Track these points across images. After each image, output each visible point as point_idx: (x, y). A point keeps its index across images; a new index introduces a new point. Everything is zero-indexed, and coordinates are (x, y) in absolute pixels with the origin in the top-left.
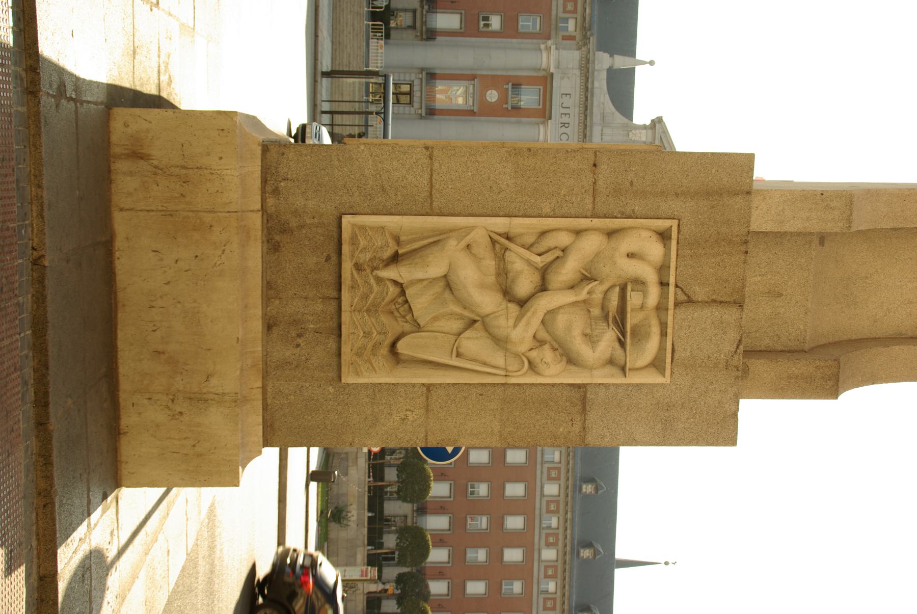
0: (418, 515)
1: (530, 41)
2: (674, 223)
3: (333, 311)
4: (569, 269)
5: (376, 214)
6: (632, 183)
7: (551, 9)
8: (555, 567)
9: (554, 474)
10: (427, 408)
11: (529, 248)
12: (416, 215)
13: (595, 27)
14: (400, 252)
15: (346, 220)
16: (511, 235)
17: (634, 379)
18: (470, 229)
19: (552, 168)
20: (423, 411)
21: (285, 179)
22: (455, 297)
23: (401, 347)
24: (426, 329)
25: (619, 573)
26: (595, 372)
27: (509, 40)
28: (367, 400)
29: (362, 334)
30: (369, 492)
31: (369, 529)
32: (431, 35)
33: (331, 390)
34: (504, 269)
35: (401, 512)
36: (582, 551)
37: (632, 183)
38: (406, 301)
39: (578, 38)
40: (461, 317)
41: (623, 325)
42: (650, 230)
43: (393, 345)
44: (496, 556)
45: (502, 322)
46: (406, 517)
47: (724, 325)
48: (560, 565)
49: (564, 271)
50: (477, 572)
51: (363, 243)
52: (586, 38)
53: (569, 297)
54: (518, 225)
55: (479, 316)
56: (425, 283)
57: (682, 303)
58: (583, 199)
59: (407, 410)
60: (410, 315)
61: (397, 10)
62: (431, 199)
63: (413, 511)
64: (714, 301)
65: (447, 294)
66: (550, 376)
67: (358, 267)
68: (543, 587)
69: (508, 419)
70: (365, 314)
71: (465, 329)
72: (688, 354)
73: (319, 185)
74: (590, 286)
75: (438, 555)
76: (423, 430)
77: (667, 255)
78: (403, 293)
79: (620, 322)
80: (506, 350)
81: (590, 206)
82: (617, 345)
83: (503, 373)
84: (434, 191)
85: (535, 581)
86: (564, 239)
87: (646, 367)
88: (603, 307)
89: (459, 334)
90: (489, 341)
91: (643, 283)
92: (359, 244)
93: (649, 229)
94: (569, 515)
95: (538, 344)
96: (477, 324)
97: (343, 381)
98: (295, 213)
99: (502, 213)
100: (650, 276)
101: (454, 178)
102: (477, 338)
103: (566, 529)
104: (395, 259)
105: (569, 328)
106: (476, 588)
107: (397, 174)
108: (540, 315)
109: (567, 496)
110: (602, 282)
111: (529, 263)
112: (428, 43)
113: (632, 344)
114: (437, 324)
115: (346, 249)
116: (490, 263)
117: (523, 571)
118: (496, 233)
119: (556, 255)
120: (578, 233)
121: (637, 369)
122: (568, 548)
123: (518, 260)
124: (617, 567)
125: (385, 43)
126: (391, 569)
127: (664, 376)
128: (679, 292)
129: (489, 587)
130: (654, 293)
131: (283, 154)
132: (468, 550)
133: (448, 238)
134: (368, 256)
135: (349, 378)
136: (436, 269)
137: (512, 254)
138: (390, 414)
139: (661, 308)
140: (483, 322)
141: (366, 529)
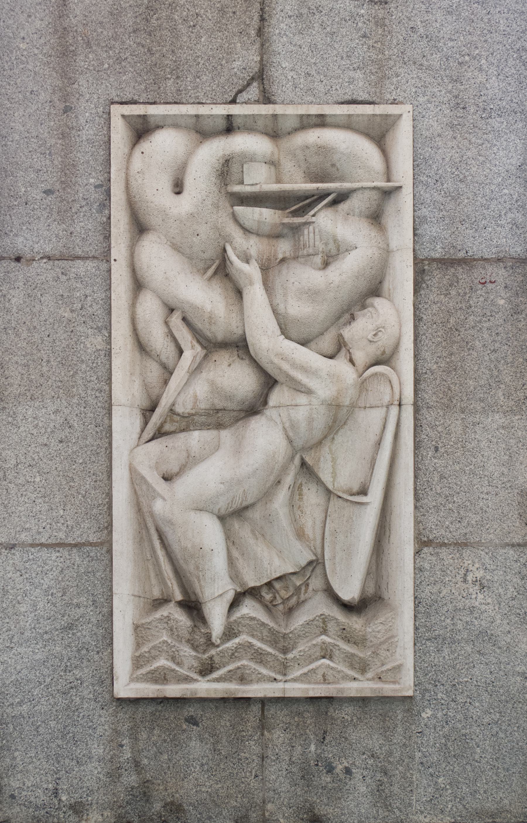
3: (285, 712)
4: (202, 296)
11: (168, 372)
14: (179, 597)
15: (125, 687)
16: (146, 404)
18: (136, 479)
19: (25, 335)
20: (466, 553)
21: (56, 793)
23: (350, 592)
24: (319, 551)
28: (446, 651)
33: (427, 713)
34: (208, 415)
38: (269, 584)
40: (297, 490)
41: (307, 198)
42: (130, 155)
43: (347, 607)
45: (300, 415)
47: (305, 11)
49: (208, 307)
51: (163, 662)
53: (256, 295)
54: (126, 389)
55: (292, 458)
56: (235, 554)
58: (78, 277)
59: (465, 581)
60: (294, 578)
62: (84, 544)
64: (260, 32)
65: (255, 514)
67: (206, 669)
69: (482, 400)
70: (290, 656)
71: (319, 482)
72: (359, 74)
73: (63, 737)
77: (175, 123)
78: (253, 593)
79: (298, 204)
80: (353, 406)
81: (90, 265)
82: (343, 207)
83: (394, 410)
84: (70, 540)
86: (149, 308)
89: (329, 492)
90: (339, 439)
92: (164, 668)
95: (343, 351)
96: (307, 459)
97: (410, 693)
98: (114, 775)
99: (106, 421)
101: (46, 507)
102: (334, 460)
104: (193, 607)
105: (313, 294)
107: (41, 605)
108: (290, 347)
111: (196, 370)
113: (342, 179)
114: (309, 531)
115: (173, 690)
116: (196, 438)
118: (142, 431)
123: (191, 391)
127: (401, 115)
131: (13, 797)
133: (152, 515)
134: (187, 651)
135: (406, 685)
136: (210, 534)
137: (180, 400)
138: (472, 610)
139: (274, 132)
140: (304, 449)
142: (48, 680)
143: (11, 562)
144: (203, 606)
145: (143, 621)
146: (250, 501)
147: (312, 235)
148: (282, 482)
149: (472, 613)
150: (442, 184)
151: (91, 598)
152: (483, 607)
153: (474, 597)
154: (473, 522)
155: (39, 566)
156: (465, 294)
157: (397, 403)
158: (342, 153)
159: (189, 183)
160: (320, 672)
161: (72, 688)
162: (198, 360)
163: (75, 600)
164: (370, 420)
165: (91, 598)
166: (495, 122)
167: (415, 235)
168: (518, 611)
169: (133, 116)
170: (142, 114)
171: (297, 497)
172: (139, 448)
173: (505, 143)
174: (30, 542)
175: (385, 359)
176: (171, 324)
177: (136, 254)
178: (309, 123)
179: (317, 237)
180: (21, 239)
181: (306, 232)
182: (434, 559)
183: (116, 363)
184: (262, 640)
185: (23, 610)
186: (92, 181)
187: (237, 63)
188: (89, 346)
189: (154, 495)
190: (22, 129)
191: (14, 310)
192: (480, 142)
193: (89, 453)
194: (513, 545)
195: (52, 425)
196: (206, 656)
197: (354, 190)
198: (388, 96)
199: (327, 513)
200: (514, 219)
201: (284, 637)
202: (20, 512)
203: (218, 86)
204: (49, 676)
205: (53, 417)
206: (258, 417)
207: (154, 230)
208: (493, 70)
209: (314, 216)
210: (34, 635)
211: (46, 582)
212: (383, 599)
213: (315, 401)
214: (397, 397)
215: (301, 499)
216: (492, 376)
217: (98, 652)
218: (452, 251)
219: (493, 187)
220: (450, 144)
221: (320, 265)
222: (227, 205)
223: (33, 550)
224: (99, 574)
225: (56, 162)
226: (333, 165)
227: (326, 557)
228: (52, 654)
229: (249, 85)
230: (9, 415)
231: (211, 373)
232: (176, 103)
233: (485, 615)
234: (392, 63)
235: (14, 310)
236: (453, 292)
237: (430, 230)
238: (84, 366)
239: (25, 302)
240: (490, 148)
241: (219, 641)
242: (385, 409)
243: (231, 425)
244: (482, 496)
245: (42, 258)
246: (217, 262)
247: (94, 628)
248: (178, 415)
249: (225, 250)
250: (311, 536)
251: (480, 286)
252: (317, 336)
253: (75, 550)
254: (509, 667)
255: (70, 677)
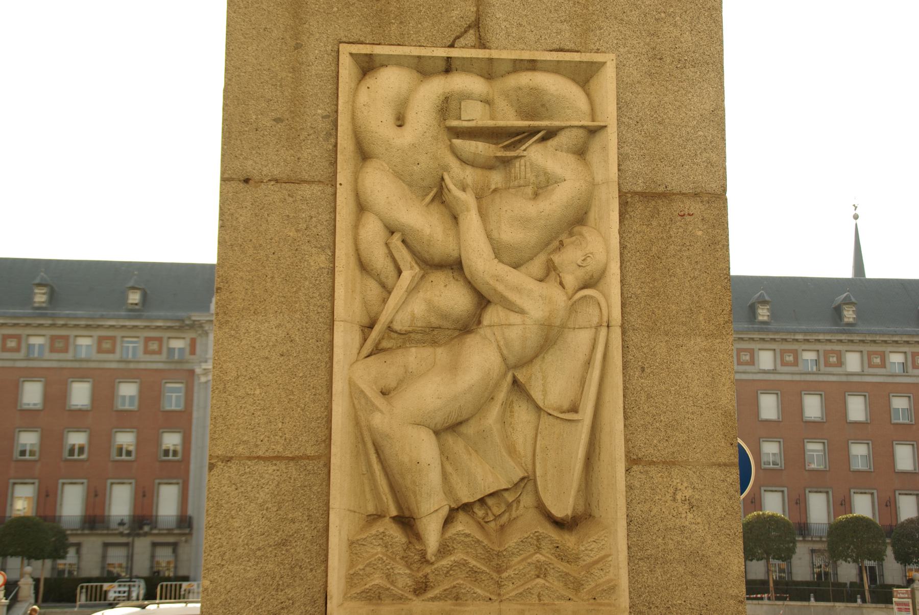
0: (809, 534)
1: (195, 395)
2: (345, 49)
5: (327, 556)
6: (278, 120)
7: (156, 370)
8: (870, 354)
9: (746, 357)
10: (669, 464)
11: (387, 290)
12: (328, 485)
13: (182, 314)
14: (394, 512)
16: (366, 321)
17: (609, 112)
20: (675, 471)
22: (473, 416)
23: (561, 510)
24: (530, 467)
25: (871, 273)
26: (599, 178)
27: (194, 421)
28: (659, 571)
29: (540, 581)
30: (785, 599)
31: (835, 600)
32: (185, 522)
34: (424, 332)
35: (807, 558)
36: (846, 320)
37: (278, 120)
38: (482, 501)
39: (193, 335)
40: (508, 406)
43: (559, 524)
44: (859, 431)
45: (514, 334)
46: (813, 551)
48: (866, 348)
49: (427, 231)
50: (883, 456)
51: (377, 580)
52: (194, 326)
53: (472, 221)
54: (348, 304)
55: (505, 375)
56: (449, 469)
57: (480, 38)
58: (303, 199)
59: (674, 500)
60: (506, 494)
61: (152, 567)
62: (301, 458)
63: (804, 541)
65: (469, 430)
66: (608, 252)
68: (898, 370)
70: (505, 575)
71: (530, 398)
72: (565, 26)
74: (451, 187)
75: (863, 506)
76: (709, 471)
78: (466, 507)
79: (512, 138)
80: (563, 327)
81: (316, 188)
83: (603, 332)
84: (288, 454)
85: (890, 380)
86: (372, 230)
87: (588, 95)
88: (488, 166)
89: (538, 409)
90: (549, 357)
91: (447, 99)
92: (380, 587)
93: (355, 92)
94: (799, 337)
95: (553, 274)
96: (521, 378)
99: (327, 336)
100: (436, 87)
102: (544, 378)
103: (819, 341)
104: (407, 522)
105: (524, 222)
106: (904, 458)
107: (255, 520)
108: (503, 270)
109: (774, 340)
110: (446, 168)
111: (413, 290)
112: (195, 526)
113: (550, 118)
114: (520, 448)
116: (414, 356)
117: (878, 396)
118: (362, 346)
119: (399, 244)
120: (361, 207)
121: (593, 109)
122: (843, 337)
123: (409, 309)
124: (864, 275)
125: (195, 580)
126: (887, 573)
127: (605, 63)
128: (462, 41)
129: (903, 441)
130: (461, 82)
132: (853, 468)
133: (370, 429)
134: (401, 569)
136: (424, 449)
137: (399, 318)
138: (682, 529)
139: (489, 71)
140: (516, 367)
141: (837, 604)
142: (259, 600)
143: (227, 475)
144: (418, 522)
145: (358, 538)
146: (465, 416)
147: (523, 168)
148: (496, 398)
149: (682, 532)
150: (643, 126)
151: (306, 513)
152: (693, 527)
153: (683, 516)
154: (680, 441)
155: (255, 480)
156: (666, 225)
157: (605, 324)
158: (552, 95)
159: (411, 116)
160: (535, 591)
161: (283, 608)
162: (416, 279)
163: (291, 515)
164: (580, 340)
165: (306, 513)
166: (689, 72)
167: (619, 170)
168: (728, 532)
169: (360, 54)
170: (368, 52)
171: (509, 414)
172: (359, 363)
173: (699, 91)
174: (247, 454)
175: (592, 282)
176: (392, 246)
177: (360, 180)
178: (519, 66)
179: (528, 170)
180: (250, 162)
181: (517, 165)
182: (643, 477)
183: (340, 280)
184: (476, 557)
185: (236, 525)
186: (319, 111)
188: (312, 264)
189: (375, 408)
190: (255, 62)
191: (241, 228)
192: (676, 89)
193: (309, 367)
194: (719, 465)
195: (273, 339)
196: (420, 574)
197: (561, 129)
198: (592, 46)
199: (537, 430)
200: (708, 158)
201: (498, 555)
202: (239, 424)
203: (438, 31)
204: (260, 595)
205: (275, 331)
206: (472, 335)
207: (377, 158)
208: (686, 26)
209: (525, 150)
210: (246, 551)
211: (262, 496)
212: (594, 517)
213: (528, 321)
214: (605, 319)
215: (512, 416)
216: (693, 301)
217: (311, 570)
218: (653, 186)
219: (689, 129)
220: (648, 90)
221: (531, 196)
222: (446, 138)
223: (249, 463)
224: (315, 488)
225: (286, 94)
226: (543, 105)
227: (538, 474)
228: (265, 572)
229: (466, 32)
230: (232, 329)
231: (428, 293)
232: (399, 45)
233: (695, 535)
234: (595, 17)
235: (241, 228)
236: (655, 223)
237: (634, 166)
238: (307, 283)
239: (252, 221)
240: (685, 95)
241: (434, 558)
242: (593, 330)
243: (446, 344)
244: (687, 416)
245: (270, 180)
246: (435, 190)
247: (309, 544)
248: (396, 332)
249: (443, 179)
250: (522, 453)
251: (679, 218)
252: (528, 261)
253: (292, 464)
254: (722, 589)
255: (281, 596)
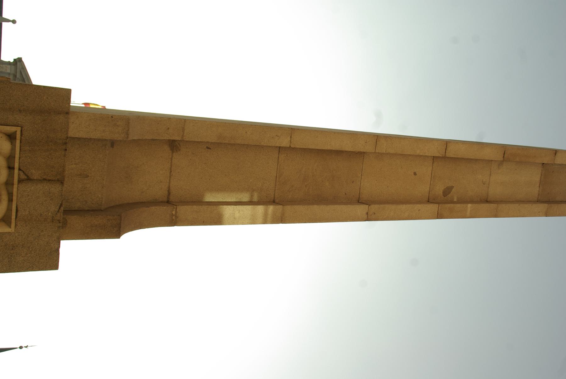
47: (51, 195)
64: (45, 179)
72: (27, 213)
127: (10, 228)
187: (34, 172)
229: (26, 175)
